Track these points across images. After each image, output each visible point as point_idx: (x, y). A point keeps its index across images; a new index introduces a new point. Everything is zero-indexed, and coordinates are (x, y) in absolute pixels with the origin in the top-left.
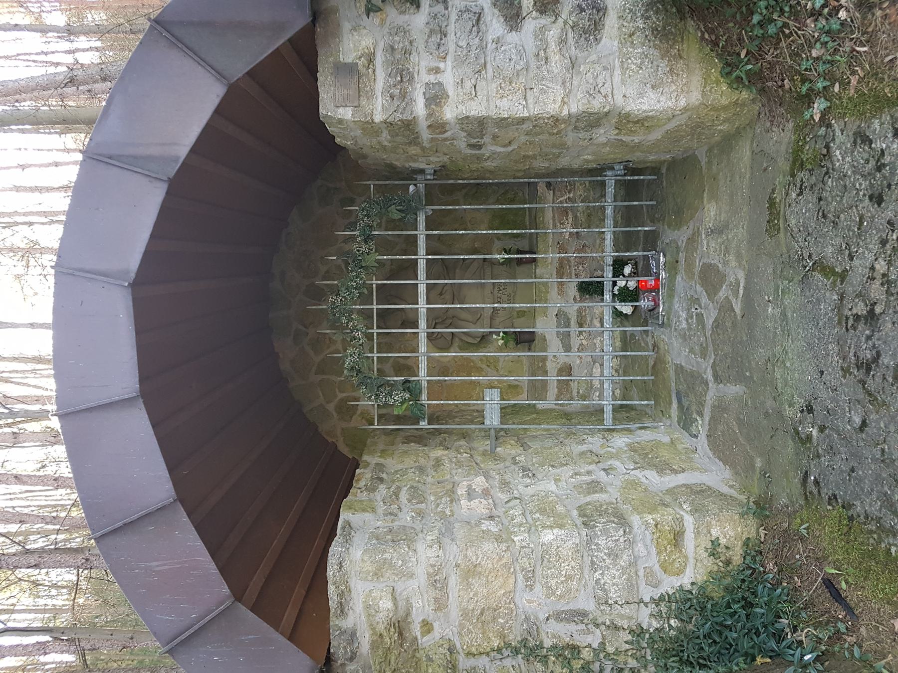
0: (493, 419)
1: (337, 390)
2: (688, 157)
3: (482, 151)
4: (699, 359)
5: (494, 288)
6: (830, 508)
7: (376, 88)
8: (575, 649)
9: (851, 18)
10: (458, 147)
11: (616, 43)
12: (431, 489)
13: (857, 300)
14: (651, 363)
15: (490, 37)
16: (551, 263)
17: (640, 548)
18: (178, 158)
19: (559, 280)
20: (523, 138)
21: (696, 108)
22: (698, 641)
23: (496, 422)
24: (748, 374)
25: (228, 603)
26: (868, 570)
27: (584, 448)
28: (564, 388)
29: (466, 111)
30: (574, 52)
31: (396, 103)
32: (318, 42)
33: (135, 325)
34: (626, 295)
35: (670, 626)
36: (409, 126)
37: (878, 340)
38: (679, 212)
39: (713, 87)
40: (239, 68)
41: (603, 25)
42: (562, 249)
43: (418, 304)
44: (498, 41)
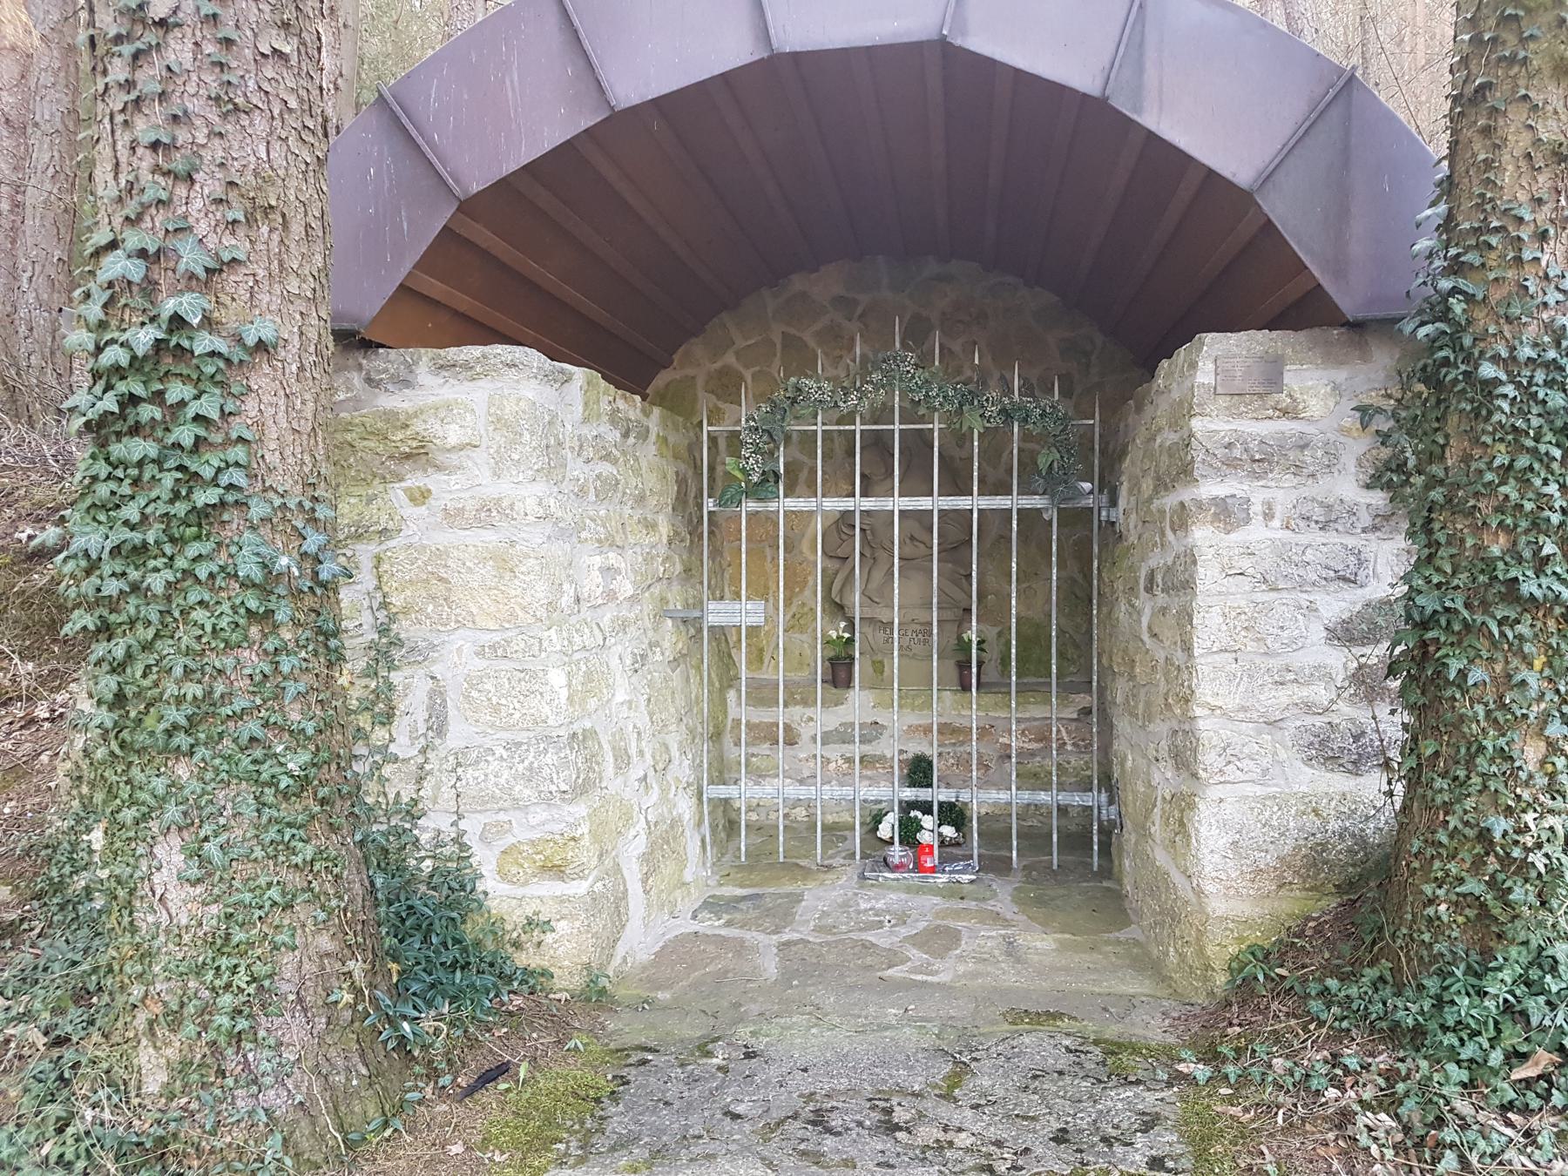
0: (718, 613)
1: (757, 368)
2: (1127, 915)
4: (812, 923)
5: (921, 624)
6: (610, 1077)
7: (1243, 422)
8: (388, 718)
9: (1327, 1103)
10: (1150, 554)
11: (1304, 789)
12: (615, 511)
13: (913, 1111)
14: (803, 862)
15: (1319, 597)
16: (959, 715)
17: (539, 815)
18: (1139, 110)
19: (935, 727)
20: (1161, 655)
21: (1202, 910)
22: (402, 898)
24: (795, 983)
25: (457, 190)
26: (527, 1116)
27: (675, 753)
28: (765, 734)
29: (1204, 561)
30: (1291, 725)
31: (1220, 452)
33: (881, 46)
34: (908, 831)
35: (423, 859)
36: (1185, 472)
37: (858, 1134)
38: (1040, 901)
39: (1232, 931)
40: (1278, 208)
41: (1332, 770)
42: (983, 732)
43: (900, 496)
44: (1312, 608)
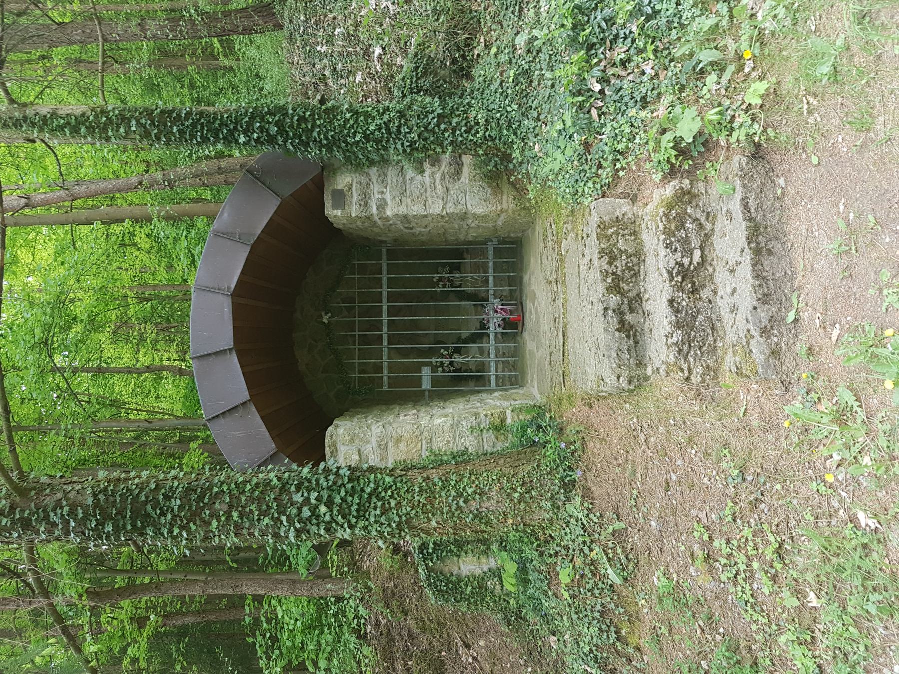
0: (426, 385)
3: (413, 231)
15: (408, 178)
23: (428, 387)
32: (324, 179)
